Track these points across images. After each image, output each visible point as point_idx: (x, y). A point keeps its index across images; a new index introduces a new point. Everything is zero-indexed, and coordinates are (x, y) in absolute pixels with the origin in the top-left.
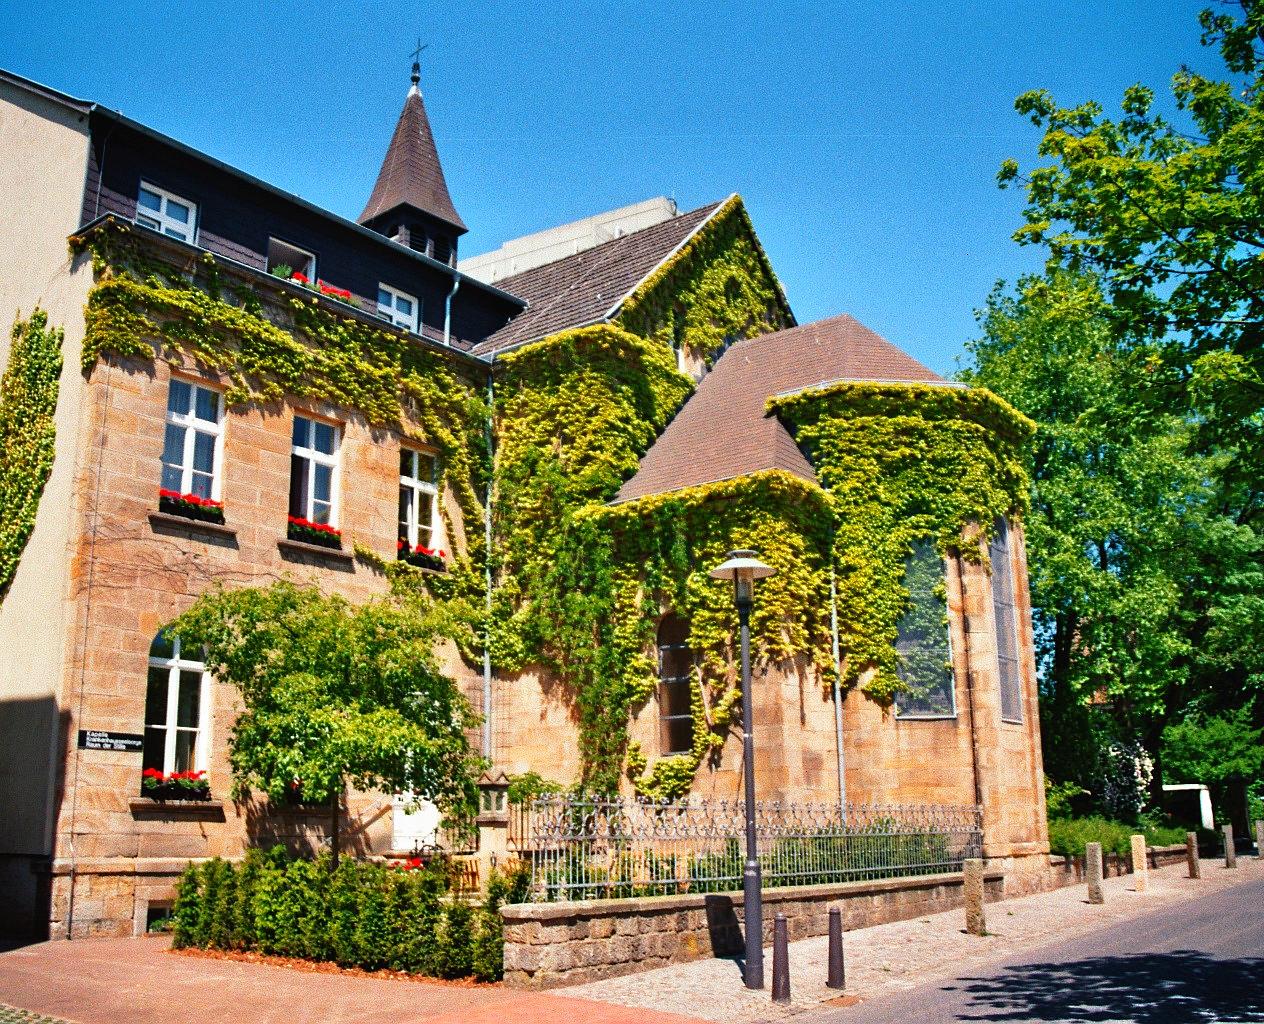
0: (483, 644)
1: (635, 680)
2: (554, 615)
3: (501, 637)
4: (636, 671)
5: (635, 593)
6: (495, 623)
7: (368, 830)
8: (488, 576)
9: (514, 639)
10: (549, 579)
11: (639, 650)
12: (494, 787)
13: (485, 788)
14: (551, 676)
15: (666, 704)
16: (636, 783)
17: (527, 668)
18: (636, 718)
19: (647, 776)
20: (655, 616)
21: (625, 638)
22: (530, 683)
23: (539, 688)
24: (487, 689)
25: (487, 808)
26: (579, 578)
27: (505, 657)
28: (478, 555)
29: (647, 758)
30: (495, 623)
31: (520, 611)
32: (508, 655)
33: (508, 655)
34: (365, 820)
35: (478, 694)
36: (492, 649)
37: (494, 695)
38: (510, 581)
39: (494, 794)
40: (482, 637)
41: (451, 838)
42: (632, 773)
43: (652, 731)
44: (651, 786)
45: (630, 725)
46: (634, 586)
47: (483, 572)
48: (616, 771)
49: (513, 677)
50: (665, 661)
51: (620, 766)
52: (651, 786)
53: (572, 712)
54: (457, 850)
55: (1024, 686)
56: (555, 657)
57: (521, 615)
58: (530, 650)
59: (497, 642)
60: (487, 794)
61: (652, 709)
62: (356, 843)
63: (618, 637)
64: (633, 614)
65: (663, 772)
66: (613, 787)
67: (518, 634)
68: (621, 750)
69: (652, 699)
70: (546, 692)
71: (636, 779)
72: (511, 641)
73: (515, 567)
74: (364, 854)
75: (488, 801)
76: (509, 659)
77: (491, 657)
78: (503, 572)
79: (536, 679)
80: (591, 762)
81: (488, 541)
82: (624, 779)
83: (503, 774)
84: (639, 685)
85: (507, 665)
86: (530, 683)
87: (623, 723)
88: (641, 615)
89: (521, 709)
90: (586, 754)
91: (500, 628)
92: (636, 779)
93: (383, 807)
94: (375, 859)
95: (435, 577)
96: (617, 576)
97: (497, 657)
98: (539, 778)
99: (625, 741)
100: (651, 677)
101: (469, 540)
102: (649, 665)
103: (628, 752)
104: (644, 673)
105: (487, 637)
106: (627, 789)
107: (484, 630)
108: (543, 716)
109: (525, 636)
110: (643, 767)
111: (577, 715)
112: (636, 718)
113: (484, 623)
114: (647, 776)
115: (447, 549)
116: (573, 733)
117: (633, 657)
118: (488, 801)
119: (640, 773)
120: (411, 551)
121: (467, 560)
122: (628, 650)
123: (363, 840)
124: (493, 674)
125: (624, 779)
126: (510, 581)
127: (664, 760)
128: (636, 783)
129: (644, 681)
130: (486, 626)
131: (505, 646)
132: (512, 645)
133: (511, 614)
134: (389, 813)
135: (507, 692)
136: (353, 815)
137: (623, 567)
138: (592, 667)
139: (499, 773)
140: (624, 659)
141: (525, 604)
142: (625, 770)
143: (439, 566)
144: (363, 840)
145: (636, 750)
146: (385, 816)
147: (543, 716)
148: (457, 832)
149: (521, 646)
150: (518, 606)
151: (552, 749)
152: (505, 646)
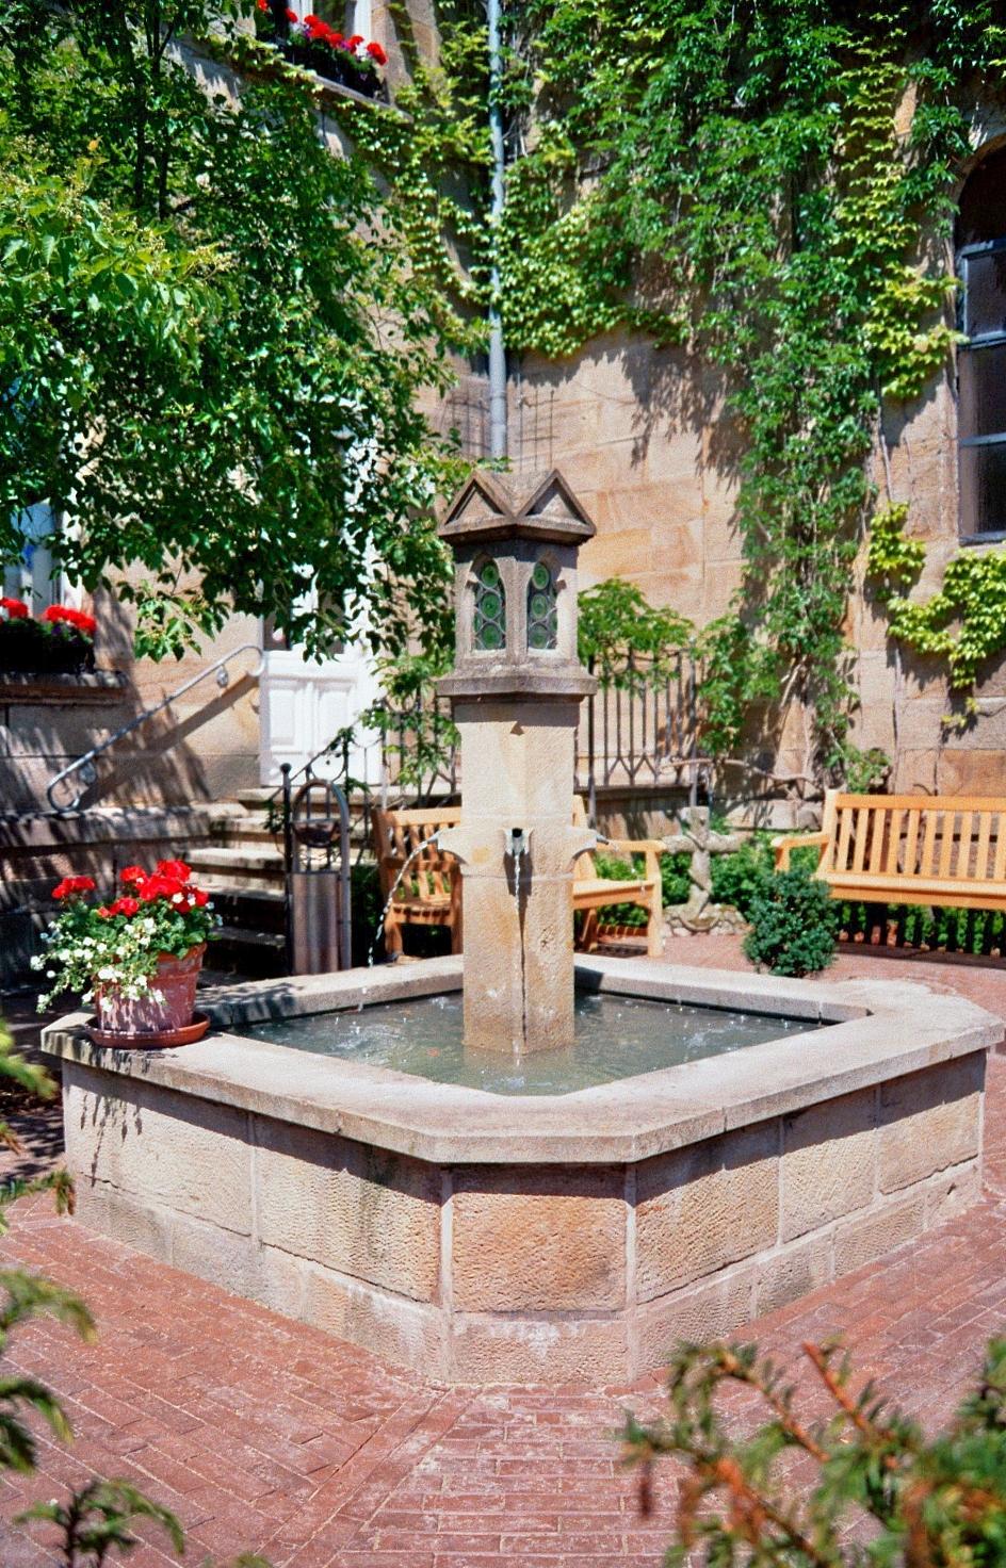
0: (486, 296)
1: (900, 335)
2: (666, 192)
3: (528, 276)
4: (900, 312)
5: (897, 102)
6: (515, 243)
7: (194, 740)
8: (495, 133)
9: (560, 274)
10: (653, 94)
11: (906, 256)
12: (515, 539)
13: (476, 547)
14: (657, 352)
15: (970, 416)
16: (893, 618)
17: (591, 341)
18: (892, 444)
19: (926, 595)
20: (958, 154)
21: (866, 225)
22: (603, 380)
23: (626, 389)
24: (497, 407)
25: (491, 633)
26: (736, 73)
27: (538, 324)
28: (471, 75)
29: (924, 548)
30: (515, 243)
31: (576, 208)
32: (546, 316)
33: (546, 316)
34: (184, 712)
35: (475, 418)
36: (507, 305)
37: (514, 419)
38: (549, 135)
39: (516, 572)
40: (483, 279)
41: (394, 757)
42: (879, 590)
43: (942, 471)
44: (937, 623)
45: (874, 463)
46: (892, 81)
47: (482, 121)
48: (836, 584)
49: (558, 368)
50: (977, 286)
51: (846, 572)
52: (937, 623)
53: (714, 442)
54: (411, 790)
55: (596, 740)
56: (668, 307)
57: (576, 217)
58: (607, 294)
59: (519, 287)
60: (486, 569)
61: (939, 419)
62: (163, 776)
63: (843, 225)
64: (886, 157)
65: (976, 583)
66: (829, 626)
67: (571, 263)
68: (849, 531)
69: (941, 389)
70: (644, 398)
71: (895, 603)
72: (554, 280)
73: (558, 98)
74: (184, 800)
75: (491, 601)
76: (548, 326)
77: (506, 328)
78: (532, 121)
79: (618, 364)
80: (772, 559)
81: (493, 46)
82: (858, 609)
83: (556, 486)
84: (905, 350)
85: (543, 340)
86: (603, 380)
87: (860, 457)
88: (910, 161)
89: (584, 446)
90: (756, 538)
91: (527, 253)
92: (895, 603)
93: (233, 680)
94: (216, 811)
95: (359, 108)
96: (848, 59)
97: (520, 326)
98: (636, 597)
99: (862, 502)
100: (940, 328)
101: (446, 35)
102: (935, 293)
103: (868, 535)
104: (920, 318)
105: (494, 281)
106: (865, 633)
107: (489, 262)
108: (638, 454)
109: (586, 261)
110: (915, 573)
111: (725, 451)
112: (892, 444)
113: (486, 246)
114: (926, 595)
115: (392, 50)
116: (722, 494)
117: (889, 274)
118: (491, 601)
119: (905, 590)
120: (296, 28)
121: (445, 88)
122: (873, 258)
123: (181, 767)
124: (509, 371)
125: (858, 609)
126: (549, 135)
127: (970, 553)
128: (893, 618)
129: (922, 341)
130: (493, 254)
131: (539, 294)
132: (555, 290)
133: (552, 217)
134: (253, 696)
135: (544, 410)
136: (150, 703)
137: (861, 28)
138: (775, 308)
139: (538, 481)
140: (864, 284)
141: (587, 188)
142: (859, 583)
143: (369, 84)
144: (181, 767)
145: (893, 527)
146: (242, 704)
147: (638, 454)
148: (411, 740)
149: (578, 290)
150: (571, 196)
151: (659, 538)
152: (539, 294)
